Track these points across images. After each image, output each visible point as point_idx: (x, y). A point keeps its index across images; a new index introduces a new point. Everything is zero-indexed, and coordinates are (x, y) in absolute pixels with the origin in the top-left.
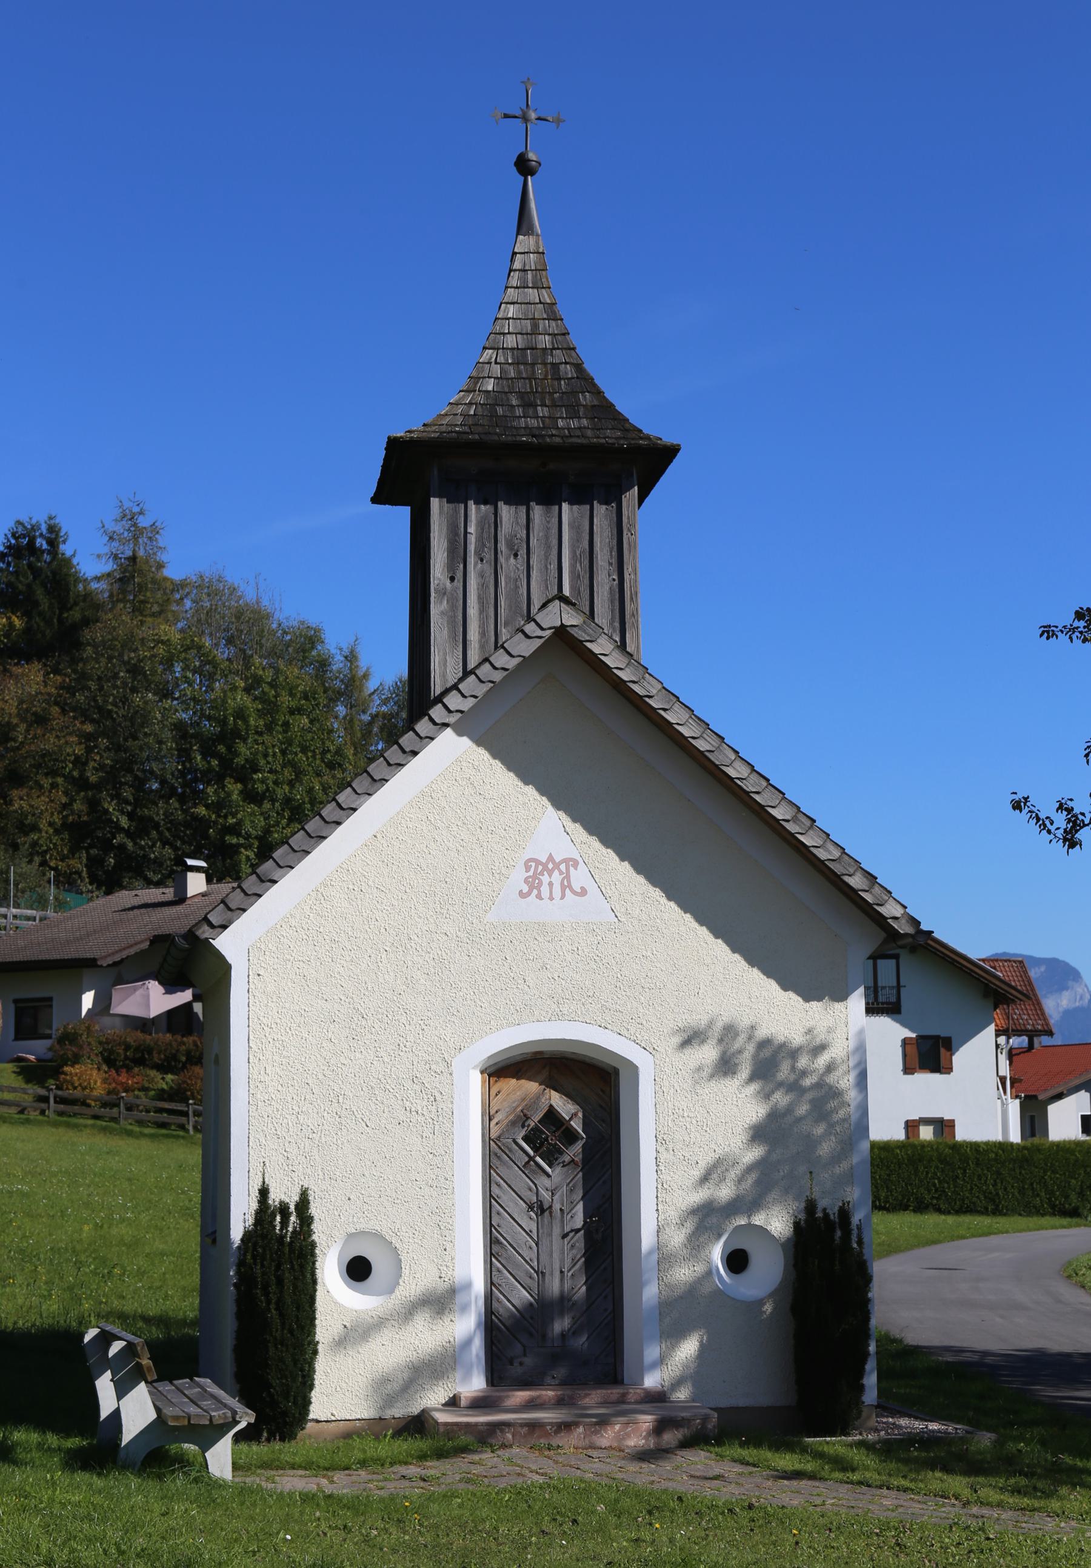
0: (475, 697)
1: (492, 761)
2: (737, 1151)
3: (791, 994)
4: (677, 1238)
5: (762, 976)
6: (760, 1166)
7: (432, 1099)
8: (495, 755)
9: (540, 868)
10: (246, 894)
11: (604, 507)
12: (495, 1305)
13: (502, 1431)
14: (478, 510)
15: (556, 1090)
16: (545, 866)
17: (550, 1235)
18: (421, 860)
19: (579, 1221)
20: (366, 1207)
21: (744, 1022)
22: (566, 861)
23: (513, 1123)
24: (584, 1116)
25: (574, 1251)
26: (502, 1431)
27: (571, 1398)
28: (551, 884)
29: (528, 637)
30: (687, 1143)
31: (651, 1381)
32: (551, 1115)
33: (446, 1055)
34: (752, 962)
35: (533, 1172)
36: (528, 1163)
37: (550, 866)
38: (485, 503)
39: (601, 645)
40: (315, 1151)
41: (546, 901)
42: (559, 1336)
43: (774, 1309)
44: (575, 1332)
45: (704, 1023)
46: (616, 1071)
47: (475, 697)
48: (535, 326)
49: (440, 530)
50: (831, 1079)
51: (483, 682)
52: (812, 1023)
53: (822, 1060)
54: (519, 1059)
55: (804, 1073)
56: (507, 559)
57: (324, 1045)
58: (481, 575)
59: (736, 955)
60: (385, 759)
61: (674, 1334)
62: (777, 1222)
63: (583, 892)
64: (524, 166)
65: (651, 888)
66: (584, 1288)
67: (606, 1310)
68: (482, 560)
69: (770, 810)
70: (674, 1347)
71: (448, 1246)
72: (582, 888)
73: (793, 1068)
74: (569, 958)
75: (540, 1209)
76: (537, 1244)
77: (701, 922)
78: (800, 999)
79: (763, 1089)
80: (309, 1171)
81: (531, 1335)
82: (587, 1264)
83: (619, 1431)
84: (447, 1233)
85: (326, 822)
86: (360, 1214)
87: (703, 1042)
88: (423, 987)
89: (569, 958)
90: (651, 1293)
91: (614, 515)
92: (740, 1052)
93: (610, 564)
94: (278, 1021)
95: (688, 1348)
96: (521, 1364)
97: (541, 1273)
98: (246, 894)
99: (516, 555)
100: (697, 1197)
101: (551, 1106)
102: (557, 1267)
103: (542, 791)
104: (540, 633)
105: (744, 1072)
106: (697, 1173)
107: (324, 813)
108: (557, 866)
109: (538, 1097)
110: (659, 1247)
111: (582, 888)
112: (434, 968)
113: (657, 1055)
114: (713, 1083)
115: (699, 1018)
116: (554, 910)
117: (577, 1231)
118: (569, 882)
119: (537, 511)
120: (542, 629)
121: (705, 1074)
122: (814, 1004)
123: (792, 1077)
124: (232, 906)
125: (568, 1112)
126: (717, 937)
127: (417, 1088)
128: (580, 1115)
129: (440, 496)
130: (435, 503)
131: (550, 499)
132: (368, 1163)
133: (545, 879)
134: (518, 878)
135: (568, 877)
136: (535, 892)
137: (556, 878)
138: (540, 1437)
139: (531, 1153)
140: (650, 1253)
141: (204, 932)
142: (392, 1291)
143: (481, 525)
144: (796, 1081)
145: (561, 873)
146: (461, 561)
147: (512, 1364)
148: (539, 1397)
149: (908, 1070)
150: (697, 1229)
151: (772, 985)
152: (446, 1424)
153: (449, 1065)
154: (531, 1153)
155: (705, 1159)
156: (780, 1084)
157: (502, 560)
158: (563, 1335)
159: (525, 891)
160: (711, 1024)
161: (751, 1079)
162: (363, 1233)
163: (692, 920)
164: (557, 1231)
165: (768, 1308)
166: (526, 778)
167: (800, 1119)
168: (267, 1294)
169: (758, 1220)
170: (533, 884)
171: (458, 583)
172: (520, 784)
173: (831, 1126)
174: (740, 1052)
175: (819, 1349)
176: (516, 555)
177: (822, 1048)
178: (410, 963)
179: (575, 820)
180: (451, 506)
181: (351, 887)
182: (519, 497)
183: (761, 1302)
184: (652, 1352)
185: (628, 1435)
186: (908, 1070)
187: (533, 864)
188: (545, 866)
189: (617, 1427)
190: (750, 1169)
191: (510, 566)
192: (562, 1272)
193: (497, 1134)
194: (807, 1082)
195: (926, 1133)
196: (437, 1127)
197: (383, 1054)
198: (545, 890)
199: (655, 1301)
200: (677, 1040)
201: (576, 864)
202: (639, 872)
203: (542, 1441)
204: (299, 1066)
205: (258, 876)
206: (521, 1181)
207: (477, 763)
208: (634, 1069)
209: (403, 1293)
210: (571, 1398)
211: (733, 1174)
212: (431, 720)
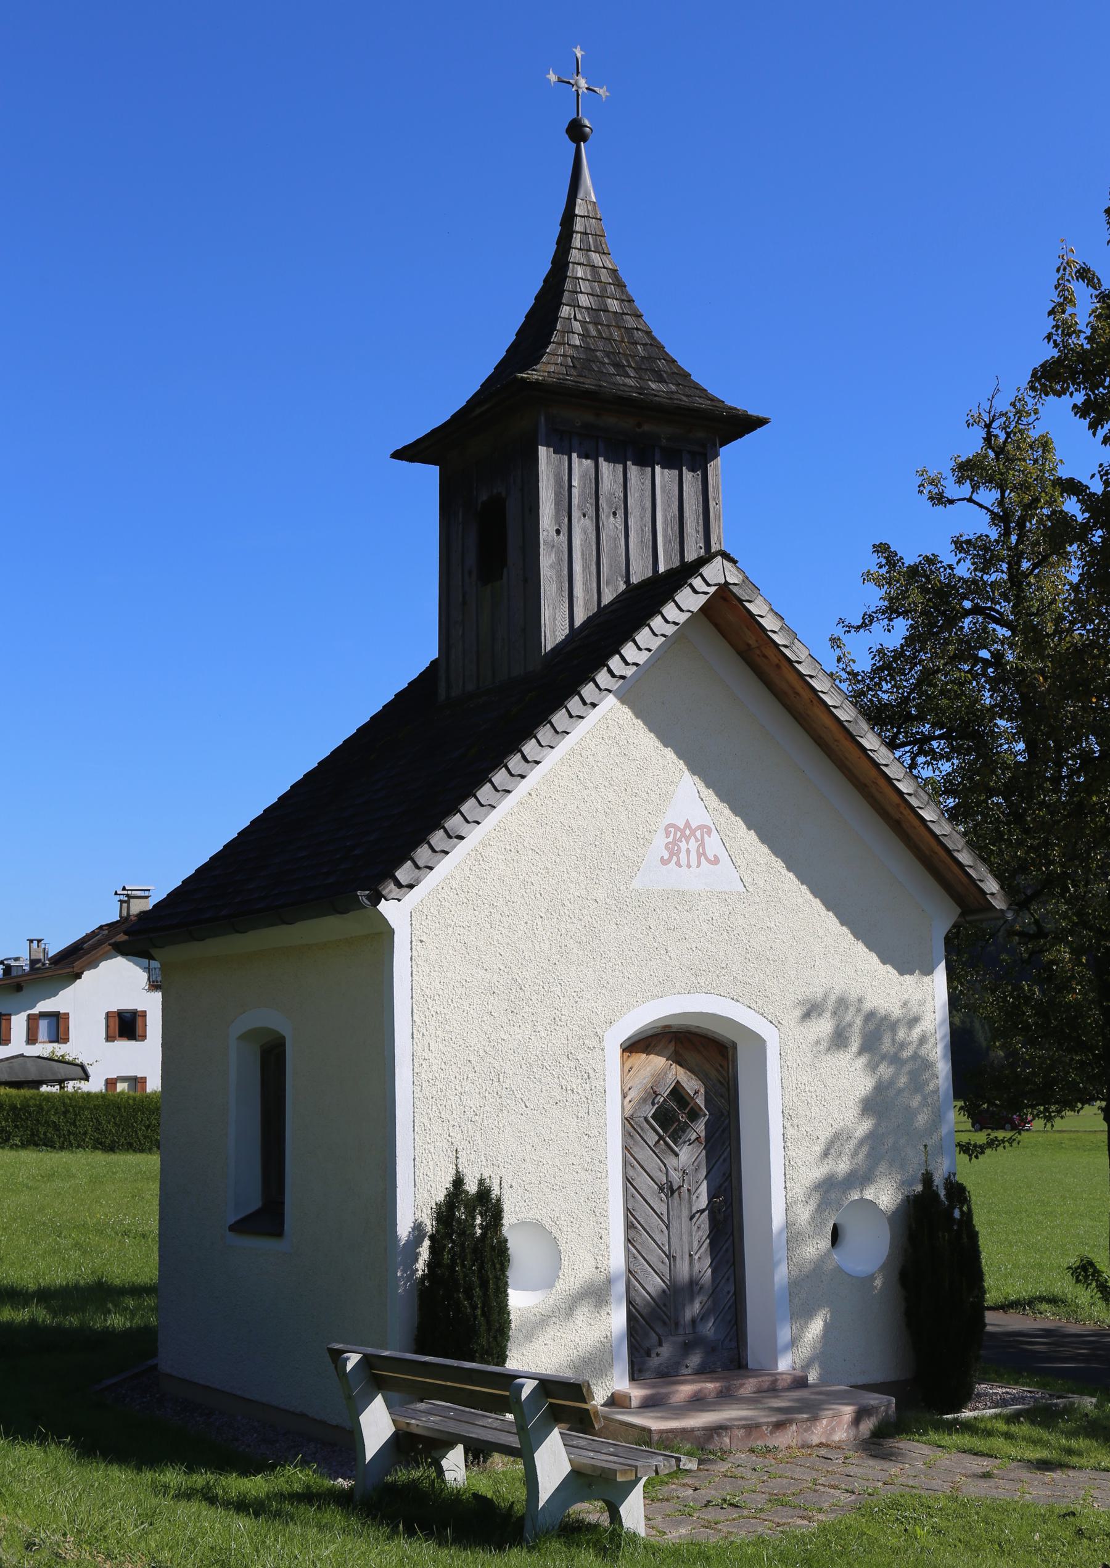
0: (649, 650)
1: (635, 721)
2: (850, 1125)
3: (889, 968)
4: (804, 1214)
5: (865, 949)
6: (871, 1138)
7: (586, 1076)
8: (638, 715)
9: (679, 834)
10: (434, 851)
11: (691, 474)
12: (633, 1293)
13: (719, 1435)
14: (580, 464)
15: (681, 1065)
16: (683, 832)
17: (680, 1217)
18: (573, 821)
19: (703, 1202)
20: (527, 1194)
21: (854, 996)
22: (701, 827)
23: (644, 1100)
24: (706, 1092)
25: (700, 1233)
26: (719, 1435)
27: (728, 1389)
28: (688, 851)
29: (695, 591)
30: (809, 1120)
31: (784, 1364)
32: (677, 1093)
33: (598, 1030)
34: (857, 935)
35: (663, 1151)
36: (658, 1142)
37: (688, 832)
38: (587, 457)
39: (758, 606)
40: (478, 1134)
41: (684, 868)
42: (694, 1323)
43: (884, 1283)
44: (703, 1317)
45: (820, 996)
46: (734, 1046)
47: (649, 650)
48: (604, 289)
49: (548, 480)
50: (923, 1051)
51: (656, 635)
52: (906, 996)
53: (916, 1032)
54: (650, 1033)
55: (902, 1046)
56: (608, 517)
57: (485, 1018)
58: (584, 531)
59: (844, 928)
60: (568, 710)
61: (803, 1313)
62: (885, 1195)
63: (716, 861)
64: (576, 132)
65: (773, 858)
66: (710, 1271)
67: (728, 1292)
68: (584, 516)
69: (896, 783)
70: (803, 1327)
71: (604, 1233)
72: (715, 856)
73: (893, 1040)
74: (705, 927)
75: (669, 1190)
76: (668, 1227)
77: (815, 894)
78: (895, 972)
79: (869, 1062)
80: (472, 1157)
81: (665, 1323)
82: (712, 1245)
83: (827, 1426)
84: (602, 1219)
85: (512, 775)
86: (521, 1203)
87: (820, 1015)
88: (575, 957)
89: (705, 927)
90: (782, 1274)
91: (700, 483)
92: (850, 1025)
93: (698, 532)
94: (441, 992)
95: (816, 1327)
96: (658, 1355)
97: (671, 1257)
98: (434, 851)
99: (615, 514)
100: (818, 1173)
101: (678, 1082)
102: (686, 1250)
103: (680, 755)
104: (706, 589)
105: (855, 1047)
106: (818, 1149)
107: (510, 765)
108: (693, 832)
109: (664, 1073)
110: (789, 1224)
111: (715, 856)
112: (585, 936)
113: (782, 1030)
114: (829, 1057)
115: (816, 991)
116: (691, 878)
117: (702, 1211)
118: (704, 849)
119: (633, 471)
120: (708, 585)
121: (825, 1044)
122: (907, 977)
123: (892, 1051)
124: (420, 863)
125: (699, 1085)
126: (828, 910)
127: (572, 1064)
128: (702, 1091)
129: (548, 445)
130: (542, 450)
131: (645, 460)
132: (528, 1147)
133: (683, 845)
134: (660, 841)
135: (702, 845)
136: (675, 858)
137: (693, 844)
138: (756, 1439)
139: (661, 1132)
140: (780, 1232)
141: (391, 891)
142: (551, 1286)
143: (583, 477)
144: (896, 1054)
145: (697, 840)
146: (566, 514)
147: (649, 1355)
148: (700, 1391)
149: (109, 1038)
150: (819, 1206)
151: (874, 958)
152: (661, 1432)
153: (600, 1040)
154: (661, 1132)
155: (825, 1134)
156: (883, 1057)
157: (603, 516)
158: (693, 1321)
159: (666, 858)
160: (826, 995)
161: (860, 1053)
162: (524, 1223)
163: (808, 892)
164: (685, 1214)
165: (878, 1282)
166: (666, 740)
167: (900, 1091)
168: (469, 1297)
169: (869, 1194)
170: (673, 850)
171: (563, 537)
172: (660, 745)
173: (925, 1098)
174: (850, 1025)
175: (935, 1323)
176: (615, 514)
177: (915, 1020)
178: (563, 931)
179: (708, 786)
180: (557, 456)
181: (508, 848)
182: (617, 457)
183: (872, 1278)
184: (784, 1334)
185: (833, 1430)
186: (109, 1038)
187: (672, 830)
188: (683, 832)
189: (825, 1422)
190: (861, 1142)
191: (612, 525)
192: (691, 1255)
193: (631, 1112)
194: (907, 1053)
195: (121, 1087)
196: (591, 1107)
197: (540, 1028)
198: (683, 855)
199: (786, 1280)
200: (798, 1013)
201: (709, 833)
202: (763, 842)
203: (759, 1443)
204: (461, 1042)
205: (446, 831)
206: (652, 1162)
207: (621, 722)
208: (759, 1043)
209: (563, 1287)
210: (728, 1389)
211: (851, 1146)
212: (610, 671)
